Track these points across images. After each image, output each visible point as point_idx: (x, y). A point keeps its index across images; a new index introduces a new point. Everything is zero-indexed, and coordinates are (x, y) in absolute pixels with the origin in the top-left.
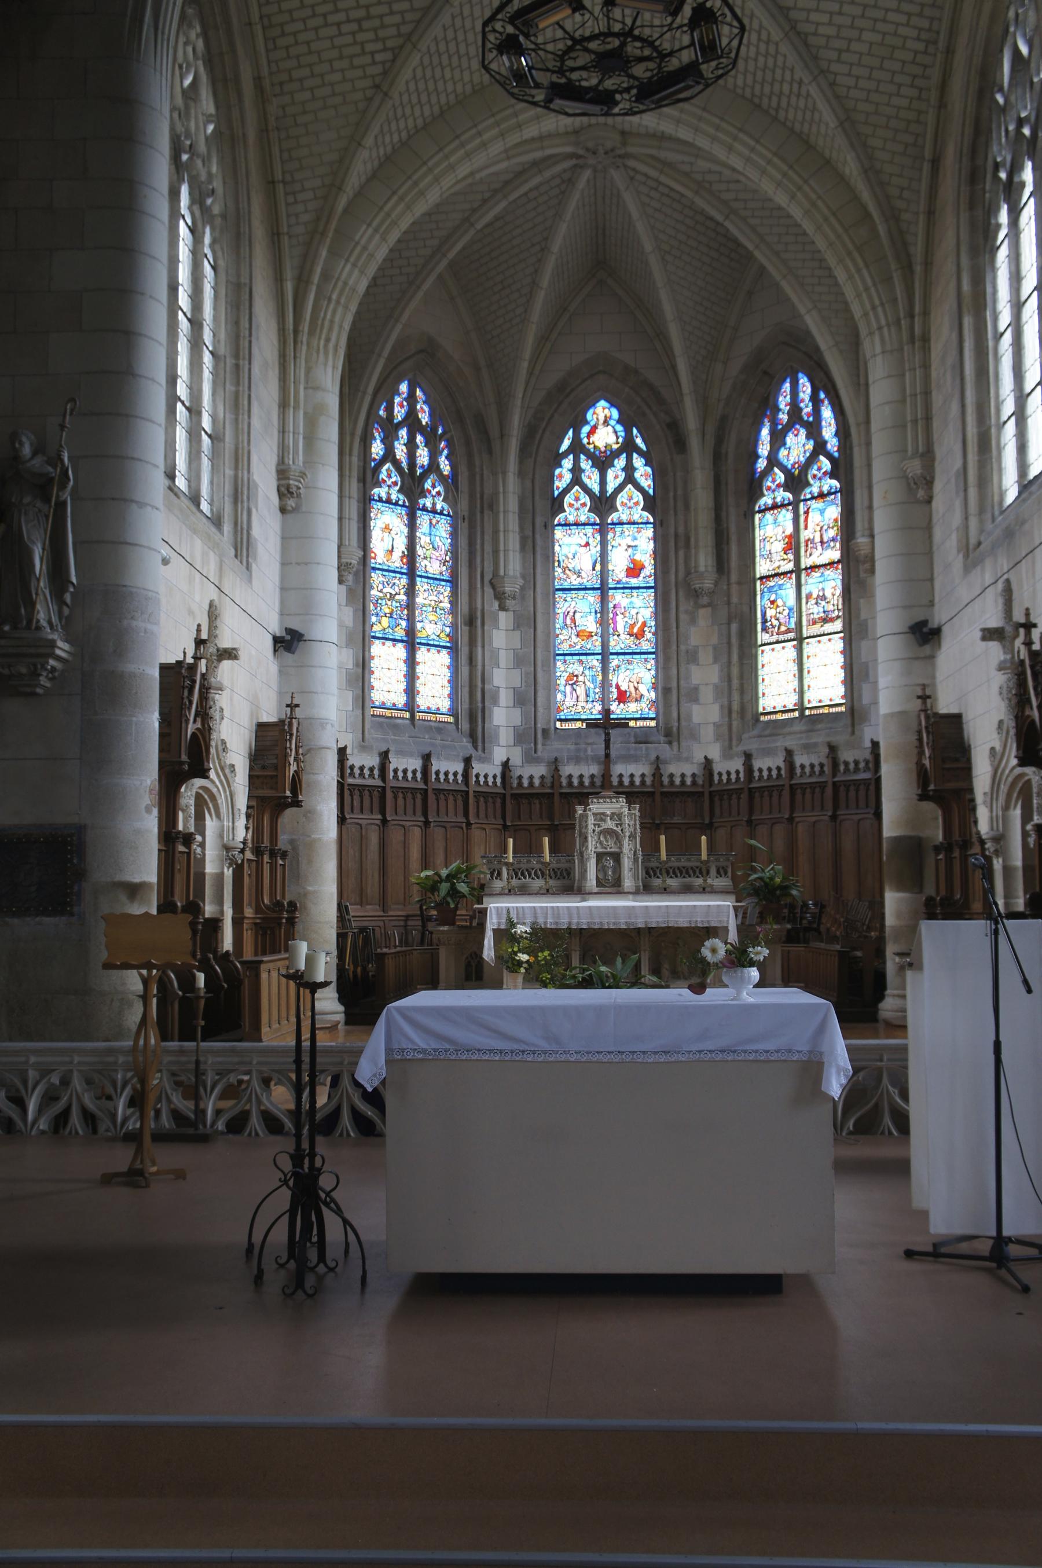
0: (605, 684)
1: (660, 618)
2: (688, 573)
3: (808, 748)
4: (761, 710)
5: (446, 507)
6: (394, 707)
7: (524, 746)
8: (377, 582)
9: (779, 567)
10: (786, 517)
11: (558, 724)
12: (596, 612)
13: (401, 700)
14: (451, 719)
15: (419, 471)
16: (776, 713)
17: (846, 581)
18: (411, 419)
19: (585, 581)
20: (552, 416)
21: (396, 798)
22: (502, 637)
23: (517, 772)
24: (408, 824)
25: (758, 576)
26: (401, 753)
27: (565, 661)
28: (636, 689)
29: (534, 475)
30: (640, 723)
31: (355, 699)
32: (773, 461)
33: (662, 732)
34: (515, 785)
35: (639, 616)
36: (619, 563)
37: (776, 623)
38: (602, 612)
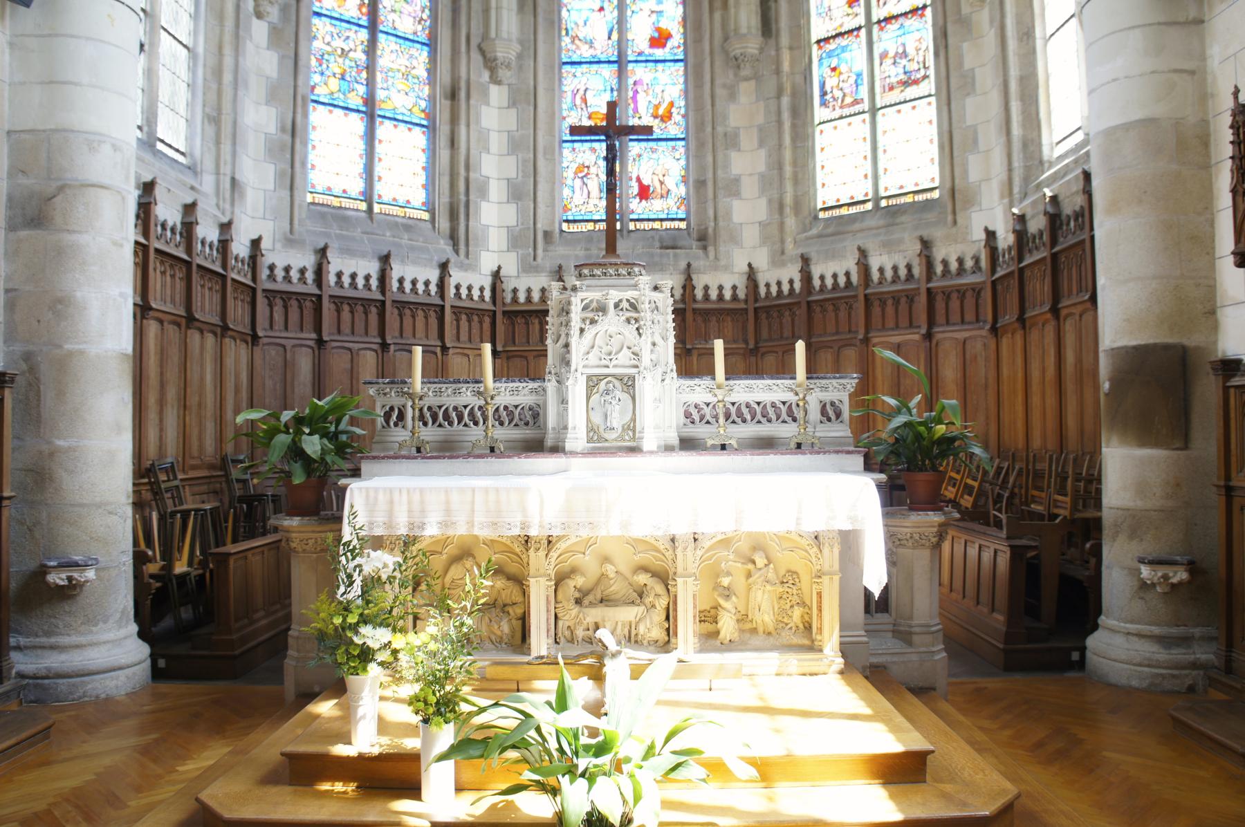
1: (691, 95)
2: (726, 38)
9: (841, 26)
11: (565, 226)
12: (612, 90)
14: (426, 216)
21: (338, 311)
22: (492, 115)
24: (356, 346)
26: (347, 252)
27: (574, 149)
28: (662, 183)
30: (667, 225)
31: (280, 175)
33: (695, 235)
37: (838, 94)
38: (619, 90)
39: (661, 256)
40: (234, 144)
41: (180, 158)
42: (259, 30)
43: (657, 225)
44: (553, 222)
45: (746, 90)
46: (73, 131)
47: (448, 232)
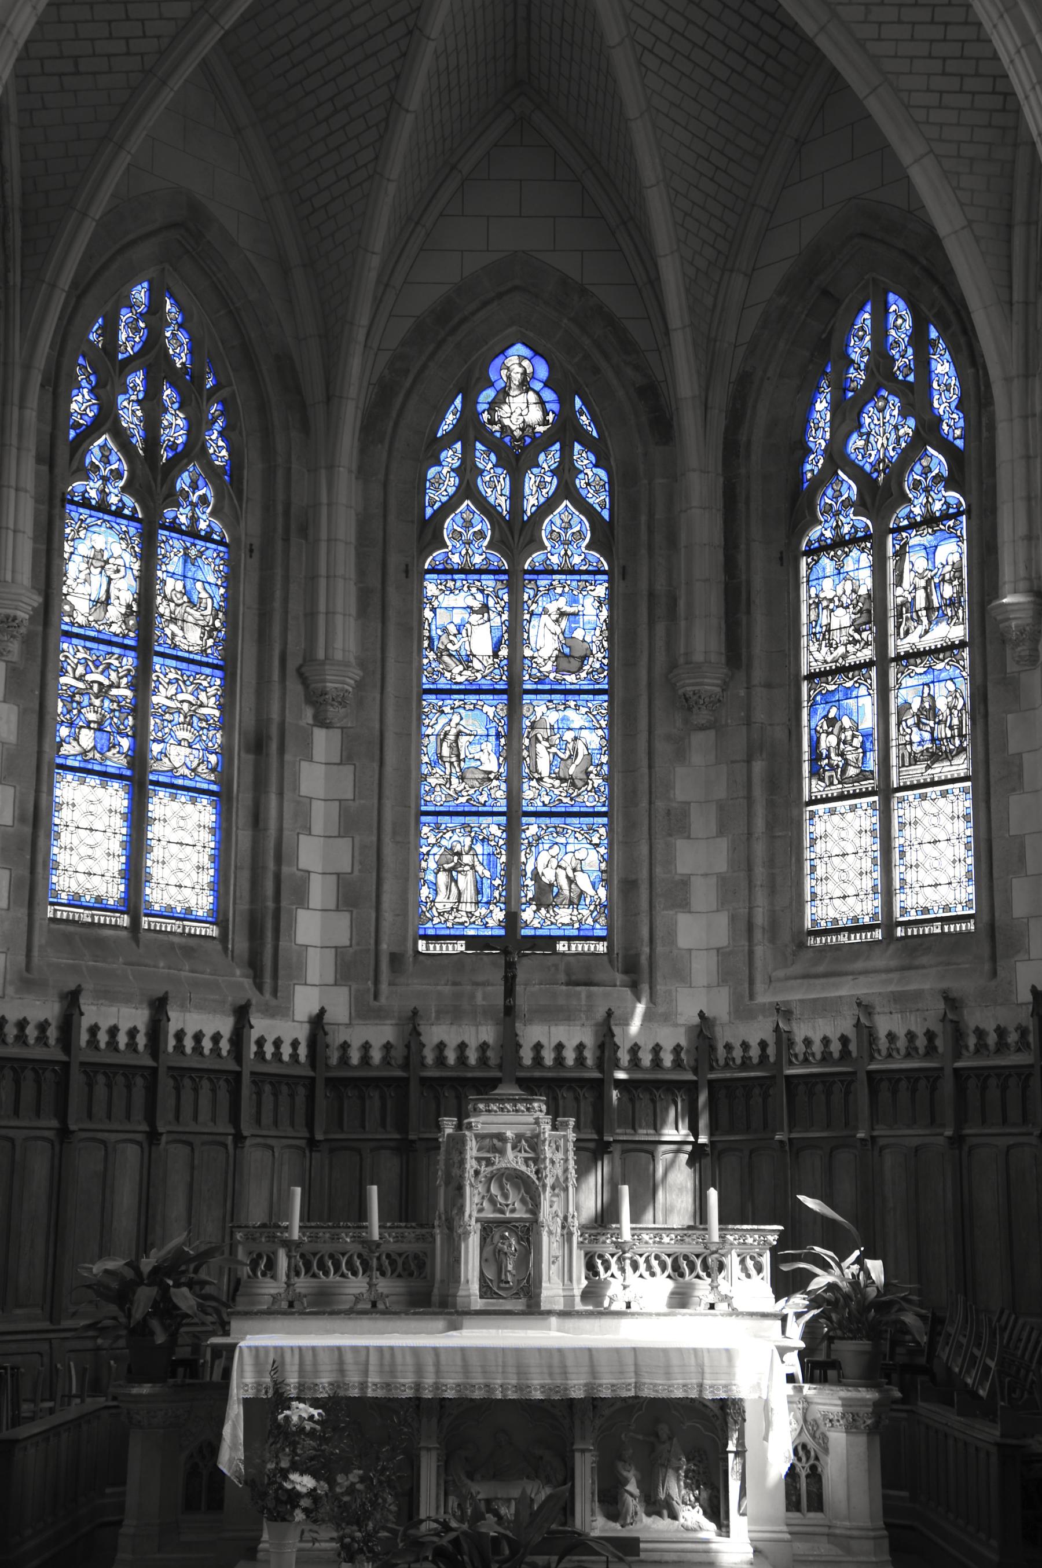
0: (513, 870)
2: (673, 666)
3: (901, 1000)
4: (808, 924)
5: (217, 525)
6: (99, 905)
9: (844, 657)
10: (859, 564)
11: (422, 946)
12: (498, 735)
13: (114, 891)
14: (213, 931)
15: (165, 455)
16: (838, 931)
17: (979, 680)
18: (153, 357)
20: (424, 367)
21: (90, 1085)
22: (318, 776)
24: (113, 1137)
25: (804, 672)
26: (108, 996)
27: (438, 826)
28: (571, 881)
29: (387, 475)
30: (577, 947)
31: (14, 886)
32: (836, 457)
34: (334, 1060)
36: (543, 639)
37: (836, 760)
44: (405, 939)
45: (701, 745)
47: (246, 956)
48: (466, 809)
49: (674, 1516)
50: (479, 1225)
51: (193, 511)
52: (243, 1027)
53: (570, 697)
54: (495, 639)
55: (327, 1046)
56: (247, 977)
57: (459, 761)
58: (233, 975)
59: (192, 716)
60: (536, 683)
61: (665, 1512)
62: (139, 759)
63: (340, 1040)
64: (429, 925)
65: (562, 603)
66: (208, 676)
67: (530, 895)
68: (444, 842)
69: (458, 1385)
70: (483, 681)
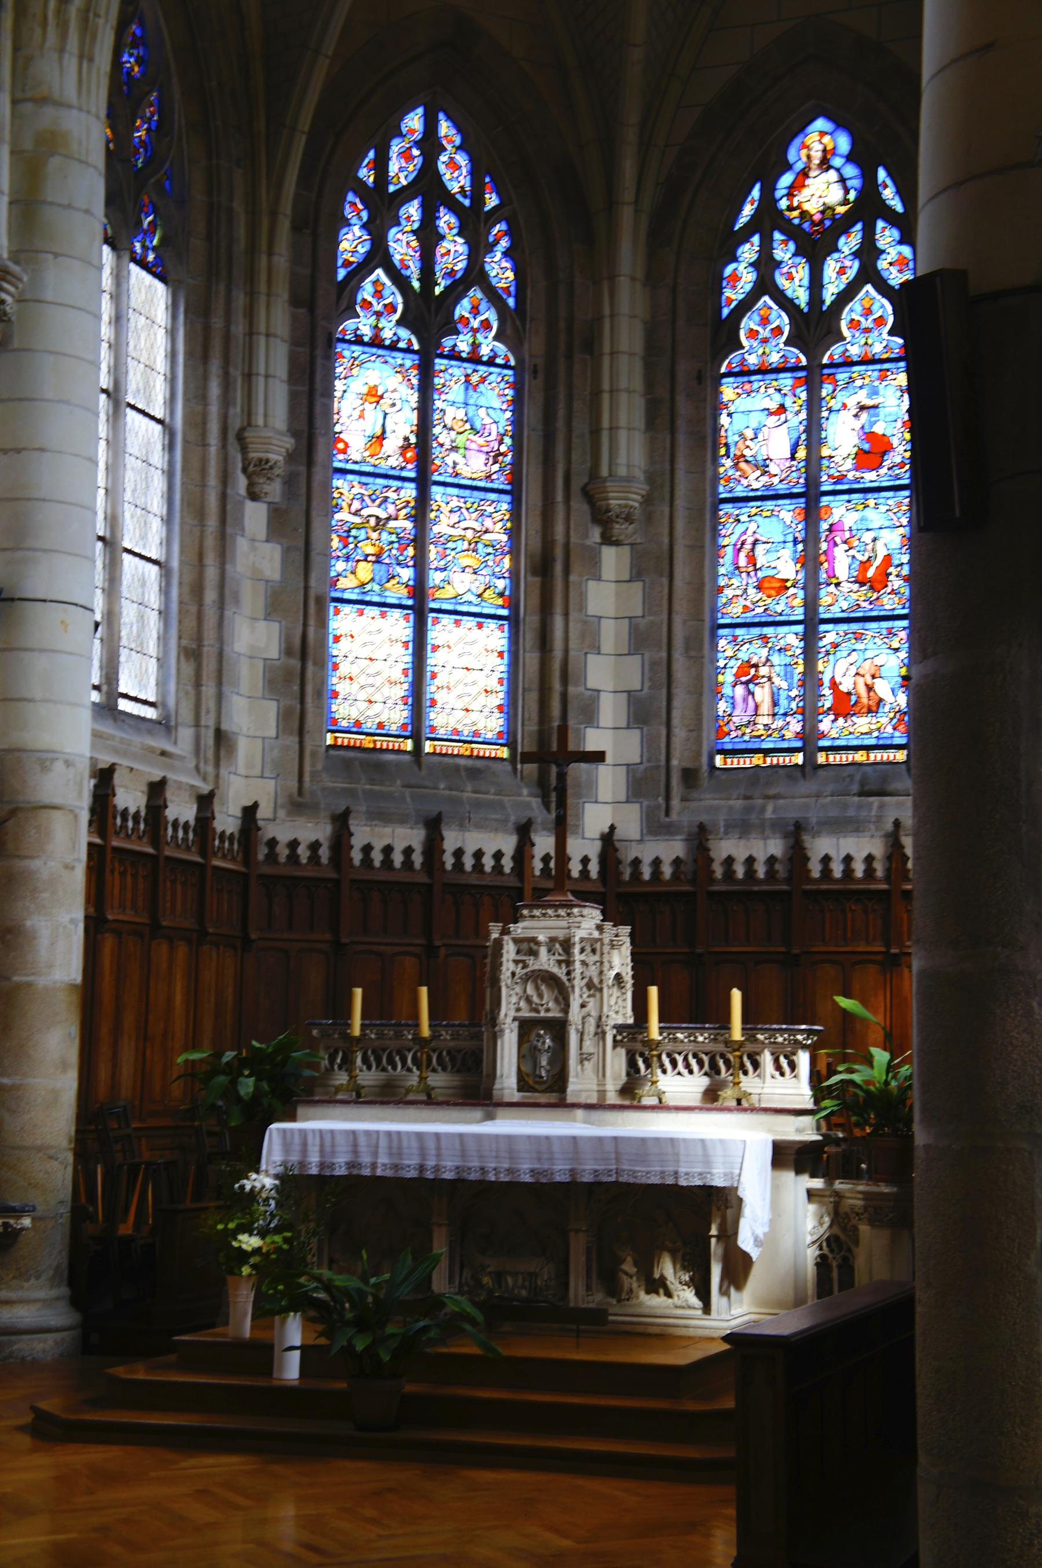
0: (810, 680)
5: (501, 348)
7: (645, 803)
8: (347, 496)
12: (795, 541)
13: (397, 716)
14: (504, 753)
18: (428, 187)
19: (776, 480)
22: (607, 594)
23: (632, 852)
26: (380, 816)
28: (870, 688)
30: (876, 756)
31: (284, 716)
34: (627, 876)
35: (879, 544)
36: (842, 437)
39: (860, 807)
40: (220, 684)
41: (150, 713)
42: (255, 516)
43: (860, 757)
44: (699, 754)
46: (25, 751)
48: (763, 619)
49: (669, 1294)
50: (516, 1023)
51: (474, 336)
52: (525, 845)
53: (869, 496)
54: (793, 441)
55: (619, 862)
56: (536, 796)
57: (756, 570)
58: (520, 795)
59: (476, 542)
60: (834, 483)
61: (661, 1291)
62: (419, 590)
63: (631, 857)
64: (727, 739)
65: (862, 397)
66: (493, 502)
67: (828, 704)
68: (740, 655)
69: (457, 1168)
70: (780, 486)
